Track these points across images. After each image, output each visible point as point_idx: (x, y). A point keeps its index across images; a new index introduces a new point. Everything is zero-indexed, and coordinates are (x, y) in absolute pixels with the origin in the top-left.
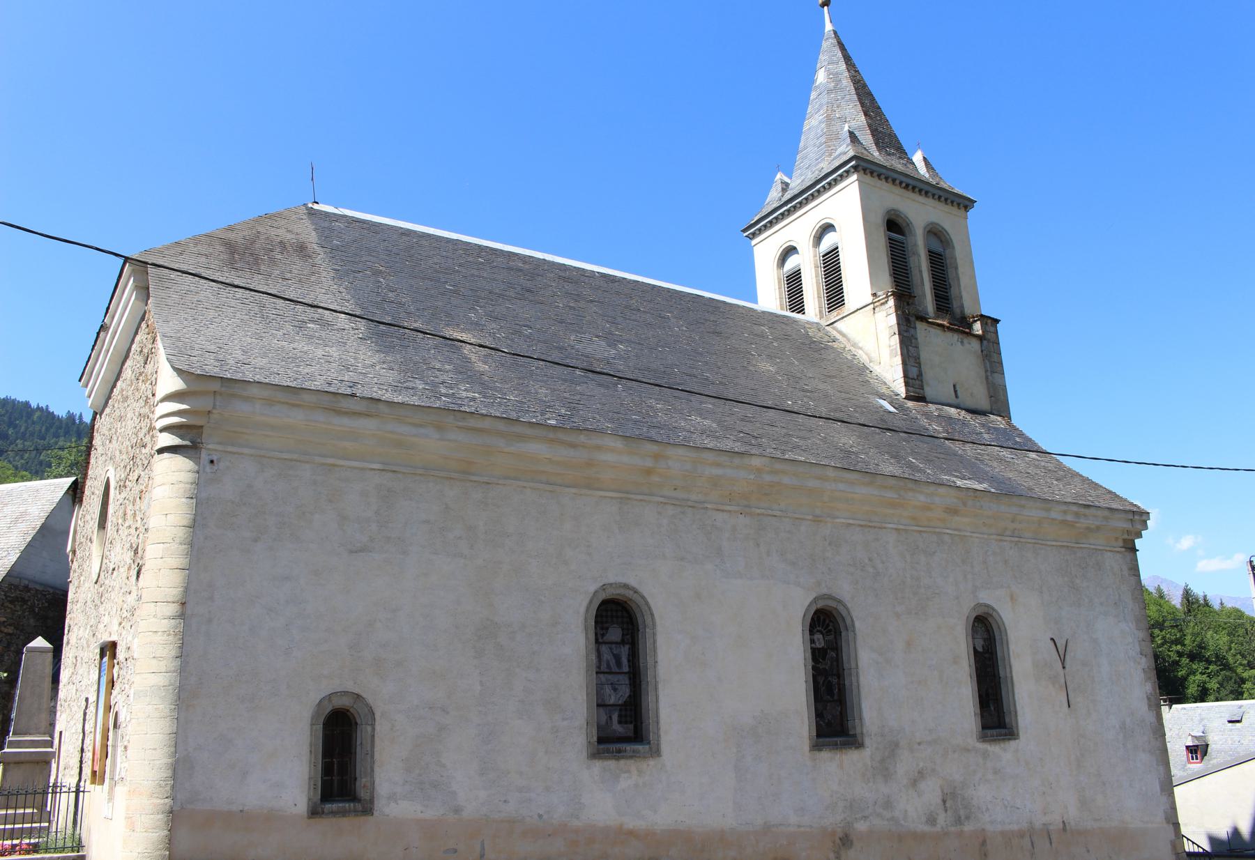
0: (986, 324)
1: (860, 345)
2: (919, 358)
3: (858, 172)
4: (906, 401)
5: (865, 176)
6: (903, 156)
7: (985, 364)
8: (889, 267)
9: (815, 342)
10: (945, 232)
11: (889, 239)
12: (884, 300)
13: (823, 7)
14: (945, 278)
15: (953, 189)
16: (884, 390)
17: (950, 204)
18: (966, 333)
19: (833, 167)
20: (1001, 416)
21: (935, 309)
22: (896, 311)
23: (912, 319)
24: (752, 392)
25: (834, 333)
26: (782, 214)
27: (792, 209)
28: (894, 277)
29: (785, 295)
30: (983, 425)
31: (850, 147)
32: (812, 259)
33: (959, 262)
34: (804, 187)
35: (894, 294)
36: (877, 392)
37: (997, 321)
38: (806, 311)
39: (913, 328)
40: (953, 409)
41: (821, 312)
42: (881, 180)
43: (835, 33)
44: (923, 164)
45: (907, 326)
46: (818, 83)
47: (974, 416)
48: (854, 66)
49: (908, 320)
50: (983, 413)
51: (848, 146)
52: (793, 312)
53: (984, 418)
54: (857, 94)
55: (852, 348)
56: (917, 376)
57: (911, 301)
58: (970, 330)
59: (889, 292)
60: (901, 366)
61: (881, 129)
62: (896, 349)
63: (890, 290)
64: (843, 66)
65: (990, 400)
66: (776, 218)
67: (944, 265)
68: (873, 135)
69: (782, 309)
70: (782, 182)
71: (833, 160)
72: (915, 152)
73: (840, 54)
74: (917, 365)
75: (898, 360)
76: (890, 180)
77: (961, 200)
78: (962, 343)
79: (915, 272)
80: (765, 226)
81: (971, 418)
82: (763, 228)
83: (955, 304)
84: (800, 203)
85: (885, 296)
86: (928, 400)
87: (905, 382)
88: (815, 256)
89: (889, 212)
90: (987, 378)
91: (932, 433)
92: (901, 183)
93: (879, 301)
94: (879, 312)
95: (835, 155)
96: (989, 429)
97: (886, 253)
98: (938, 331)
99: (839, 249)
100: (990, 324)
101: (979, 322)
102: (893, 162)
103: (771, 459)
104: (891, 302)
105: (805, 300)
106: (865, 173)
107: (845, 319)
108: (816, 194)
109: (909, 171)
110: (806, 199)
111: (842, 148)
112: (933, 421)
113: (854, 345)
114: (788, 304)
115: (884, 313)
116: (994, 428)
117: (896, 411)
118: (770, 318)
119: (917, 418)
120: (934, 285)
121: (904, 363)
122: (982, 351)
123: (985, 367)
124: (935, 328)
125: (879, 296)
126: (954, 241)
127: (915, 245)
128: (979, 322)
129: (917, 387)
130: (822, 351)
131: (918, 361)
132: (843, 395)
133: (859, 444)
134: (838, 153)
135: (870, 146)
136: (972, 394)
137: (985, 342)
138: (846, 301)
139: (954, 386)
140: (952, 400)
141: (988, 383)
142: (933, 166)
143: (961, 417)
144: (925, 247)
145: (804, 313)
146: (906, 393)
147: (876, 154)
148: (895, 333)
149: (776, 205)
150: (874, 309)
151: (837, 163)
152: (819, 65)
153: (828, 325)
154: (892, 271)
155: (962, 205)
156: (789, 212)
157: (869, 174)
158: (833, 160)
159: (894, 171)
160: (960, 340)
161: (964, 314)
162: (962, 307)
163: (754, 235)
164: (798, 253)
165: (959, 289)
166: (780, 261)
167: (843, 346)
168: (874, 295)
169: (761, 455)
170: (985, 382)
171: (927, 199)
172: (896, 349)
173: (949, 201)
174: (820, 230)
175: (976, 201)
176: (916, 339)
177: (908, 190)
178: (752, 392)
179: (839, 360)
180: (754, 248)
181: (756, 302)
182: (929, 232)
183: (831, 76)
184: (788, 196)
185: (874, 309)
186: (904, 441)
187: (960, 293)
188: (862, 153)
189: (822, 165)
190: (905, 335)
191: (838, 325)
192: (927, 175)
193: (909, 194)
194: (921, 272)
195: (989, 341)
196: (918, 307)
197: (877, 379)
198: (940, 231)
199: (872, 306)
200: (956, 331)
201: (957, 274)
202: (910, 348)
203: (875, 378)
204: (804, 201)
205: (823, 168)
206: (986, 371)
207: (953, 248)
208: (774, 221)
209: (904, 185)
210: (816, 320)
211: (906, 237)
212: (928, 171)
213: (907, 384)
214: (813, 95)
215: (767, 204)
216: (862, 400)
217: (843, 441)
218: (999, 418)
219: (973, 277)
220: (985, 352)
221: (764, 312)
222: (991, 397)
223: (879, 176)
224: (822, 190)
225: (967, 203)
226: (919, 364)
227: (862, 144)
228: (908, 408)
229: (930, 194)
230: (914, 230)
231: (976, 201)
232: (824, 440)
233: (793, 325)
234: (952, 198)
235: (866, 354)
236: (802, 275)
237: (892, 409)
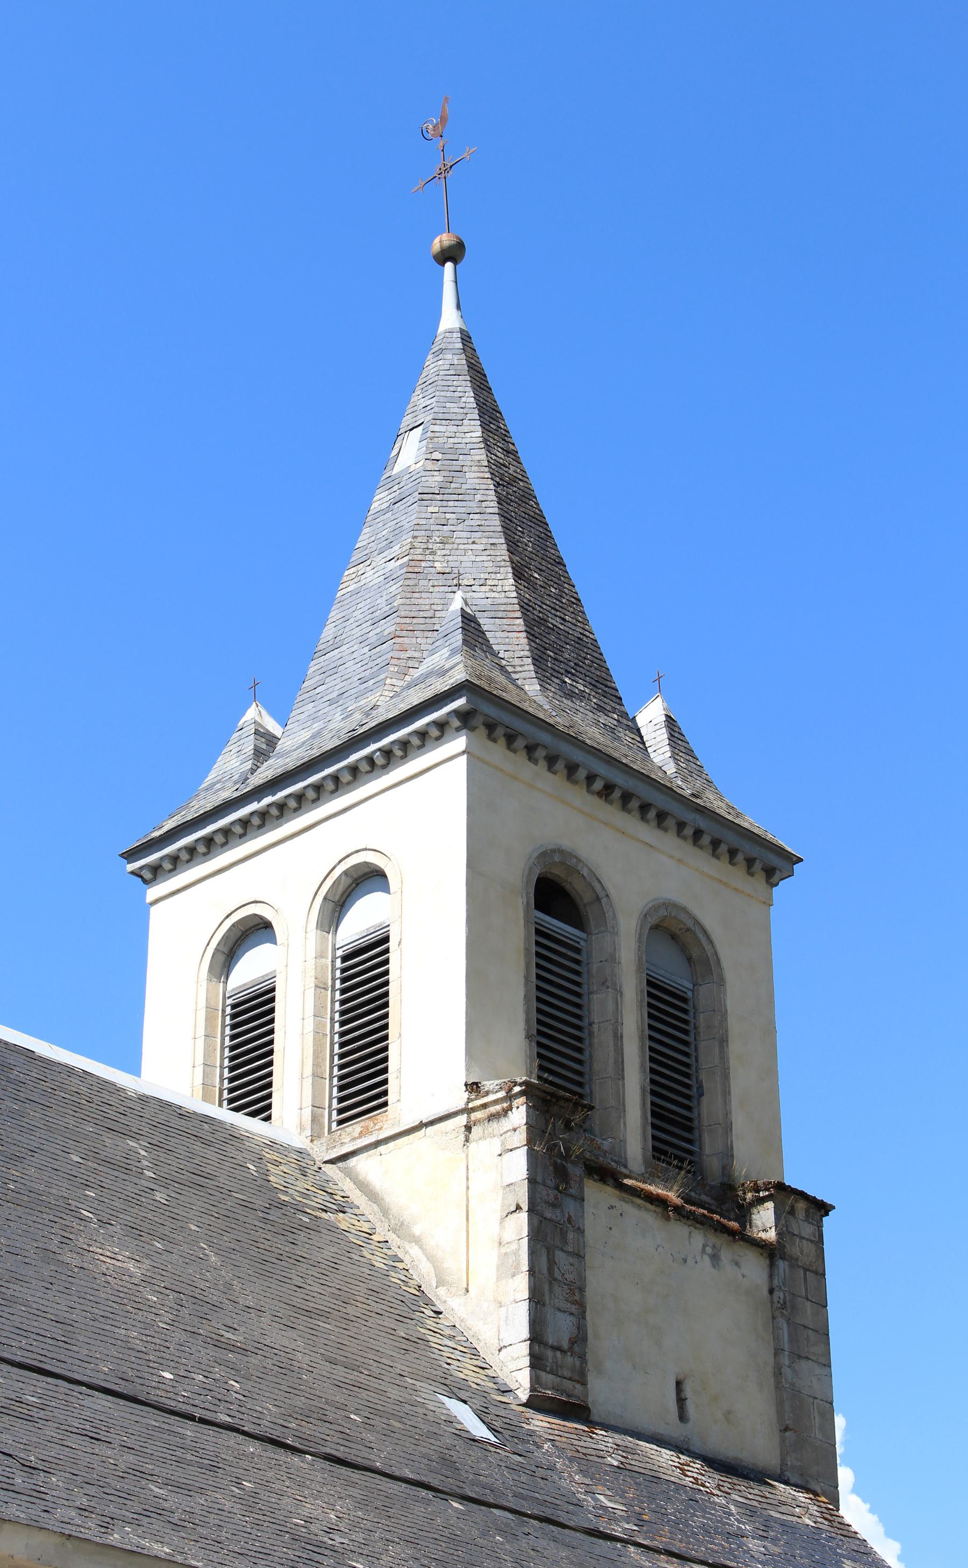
0: (792, 1212)
1: (417, 1230)
2: (582, 1290)
3: (472, 729)
4: (530, 1413)
5: (714, 861)
6: (610, 704)
7: (775, 1329)
8: (527, 1013)
9: (284, 1204)
10: (700, 935)
11: (538, 932)
12: (498, 1108)
13: (443, 264)
14: (688, 1065)
15: (738, 815)
16: (466, 1371)
17: (726, 857)
18: (731, 1233)
19: (404, 707)
20: (808, 1490)
21: (650, 1153)
22: (530, 1142)
23: (576, 1171)
24: (57, 1331)
25: (347, 1186)
26: (245, 823)
27: (274, 812)
28: (539, 1044)
29: (221, 1058)
30: (750, 1512)
31: (458, 658)
32: (311, 963)
33: (734, 1026)
34: (316, 752)
35: (529, 1091)
36: (445, 1376)
37: (823, 1208)
38: (275, 1111)
39: (574, 1198)
40: (666, 1454)
41: (315, 1119)
42: (536, 762)
43: (466, 338)
44: (663, 735)
45: (557, 1188)
46: (395, 471)
47: (728, 1481)
48: (505, 436)
49: (562, 1174)
50: (757, 1476)
51: (453, 653)
52: (237, 1109)
53: (756, 1489)
54: (504, 516)
55: (391, 1237)
56: (572, 1342)
57: (577, 1118)
58: (743, 1226)
59: (515, 1084)
60: (525, 1306)
61: (557, 622)
62: (516, 1253)
63: (519, 1080)
64: (475, 432)
65: (783, 1441)
66: (226, 832)
67: (690, 1028)
68: (531, 635)
69: (206, 1098)
70: (257, 732)
71: (409, 687)
72: (642, 702)
73: (469, 399)
74: (574, 1308)
75: (520, 1286)
76: (560, 765)
77: (755, 851)
78: (715, 1258)
79: (602, 1040)
80: (191, 850)
81: (718, 1487)
82: (184, 856)
83: (709, 1147)
84: (300, 797)
85: (501, 1094)
86: (595, 1417)
87: (532, 1355)
88: (320, 955)
89: (545, 855)
90: (778, 1372)
91: (591, 1521)
92: (591, 778)
93: (484, 1106)
94: (483, 1138)
95: (416, 674)
96: (767, 1523)
97: (522, 973)
98: (648, 1217)
99: (392, 944)
100: (801, 1215)
101: (770, 1205)
102: (578, 718)
103: (57, 1540)
104: (519, 1115)
105: (275, 1078)
106: (491, 737)
107: (382, 1149)
108: (346, 777)
109: (621, 749)
110: (318, 788)
111: (439, 658)
112: (599, 1482)
113: (399, 1228)
114: (226, 1084)
115: (495, 1145)
116: (783, 1524)
117: (493, 1439)
118: (162, 1118)
119: (552, 1468)
120: (652, 1081)
121: (536, 1299)
122: (771, 1291)
123: (776, 1338)
124: (639, 1207)
125: (487, 1093)
126: (725, 964)
127: (613, 959)
128: (770, 1205)
129: (567, 1373)
130: (302, 1237)
131: (577, 1297)
132: (340, 1372)
133: (354, 1526)
134: (423, 669)
135: (517, 662)
136: (728, 1414)
137: (782, 1265)
138: (391, 1098)
139: (679, 1384)
140: (670, 1425)
141: (778, 1387)
142: (692, 745)
143: (688, 1481)
144: (639, 969)
145: (268, 1119)
146: (532, 1389)
147: (532, 688)
148: (518, 1208)
149: (227, 794)
150: (468, 1128)
151: (415, 698)
152: (407, 421)
153: (332, 1162)
154: (535, 1025)
155: (758, 866)
156: (265, 819)
157: (502, 741)
158: (409, 687)
159: (577, 742)
160: (709, 1250)
161: (730, 1176)
162: (728, 1154)
163: (156, 873)
164: (273, 940)
165: (726, 1102)
166: (221, 958)
167: (366, 1227)
168: (473, 1087)
169: (34, 1526)
170: (772, 1381)
171: (660, 833)
172: (516, 1253)
173: (723, 848)
174: (346, 882)
175: (800, 860)
176: (580, 1231)
177: (611, 803)
178: (57, 1331)
179: (346, 1268)
180: (153, 910)
181: (135, 1069)
182: (656, 927)
183: (437, 455)
184: (267, 772)
185: (468, 1128)
186: (501, 1532)
187: (727, 1114)
188: (490, 680)
189: (372, 699)
190: (548, 1215)
191: (362, 1164)
192: (671, 769)
193: (611, 813)
194: (618, 1038)
195: (793, 1262)
196: (600, 1141)
197: (452, 1337)
198: (688, 930)
199: (462, 1120)
200: (702, 1223)
201: (724, 1058)
202: (560, 1256)
203: (448, 1332)
204: (311, 794)
205: (374, 707)
206: (778, 1352)
207: (722, 982)
208: (219, 839)
209: (598, 785)
210: (299, 1140)
211: (589, 933)
212: (674, 757)
213: (536, 1362)
214: (380, 500)
215: (207, 789)
216: (394, 1393)
217: (308, 1509)
218: (802, 1497)
219: (770, 1071)
220: (778, 1294)
221: (144, 1099)
222: (786, 1429)
223: (530, 750)
224: (364, 767)
225: (774, 861)
226: (582, 1305)
227: (495, 654)
228: (531, 1433)
229: (670, 822)
230: (614, 917)
231: (800, 860)
232: (250, 1502)
233: (229, 1148)
234: (732, 839)
235: (431, 1258)
236: (278, 1005)
237: (480, 1431)
